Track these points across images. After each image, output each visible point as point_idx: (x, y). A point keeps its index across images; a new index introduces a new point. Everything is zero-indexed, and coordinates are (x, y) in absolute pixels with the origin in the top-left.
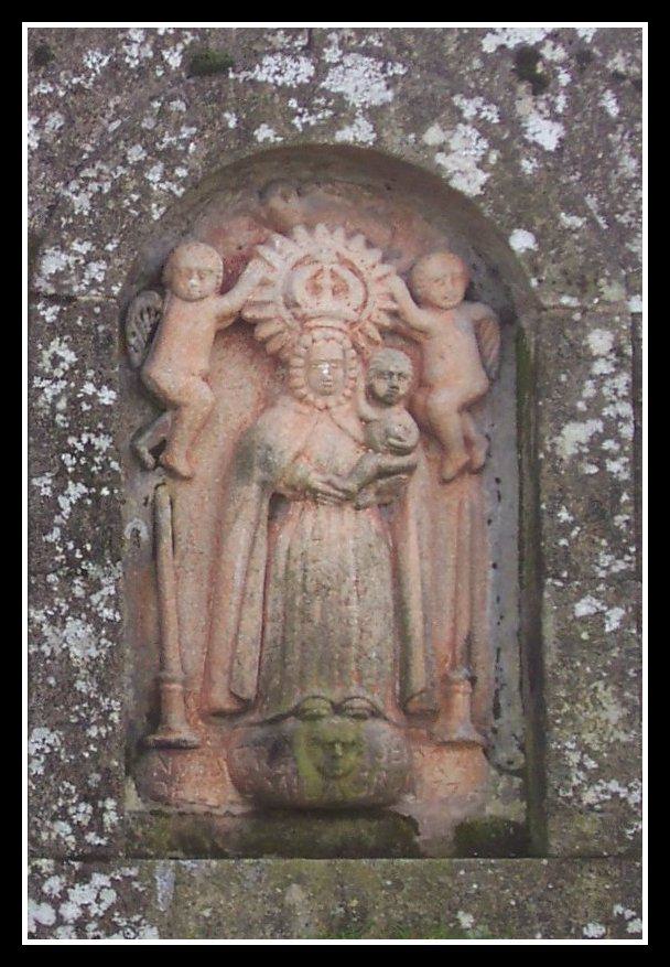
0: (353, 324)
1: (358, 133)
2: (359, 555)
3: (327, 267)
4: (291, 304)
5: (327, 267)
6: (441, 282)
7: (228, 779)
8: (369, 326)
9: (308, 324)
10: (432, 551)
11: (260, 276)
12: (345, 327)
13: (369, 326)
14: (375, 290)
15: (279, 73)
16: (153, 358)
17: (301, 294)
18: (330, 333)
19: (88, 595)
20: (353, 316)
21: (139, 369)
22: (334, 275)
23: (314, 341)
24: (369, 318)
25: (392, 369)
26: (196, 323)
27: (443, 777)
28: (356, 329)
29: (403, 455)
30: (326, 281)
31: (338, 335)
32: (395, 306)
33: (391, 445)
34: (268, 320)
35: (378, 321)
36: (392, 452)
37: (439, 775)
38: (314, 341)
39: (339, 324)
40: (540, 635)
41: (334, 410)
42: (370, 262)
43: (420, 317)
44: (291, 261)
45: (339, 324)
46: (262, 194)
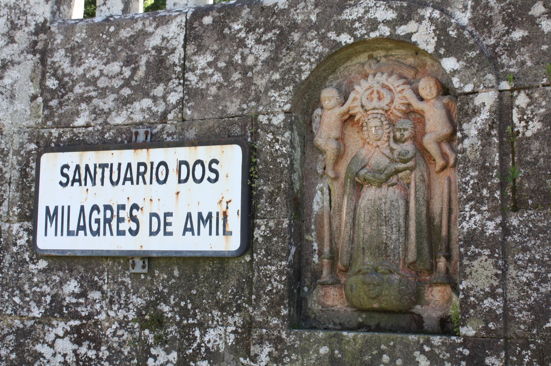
0: (386, 111)
1: (386, 31)
2: (387, 205)
3: (375, 89)
4: (362, 106)
5: (375, 89)
8: (394, 111)
10: (417, 200)
12: (383, 112)
13: (394, 111)
14: (397, 96)
15: (351, 15)
17: (365, 102)
18: (375, 115)
20: (387, 108)
22: (378, 92)
23: (368, 119)
25: (401, 127)
27: (433, 298)
28: (389, 113)
29: (405, 163)
30: (375, 95)
34: (357, 113)
36: (401, 162)
37: (431, 297)
38: (368, 119)
39: (380, 111)
40: (416, 239)
41: (380, 146)
42: (396, 84)
43: (417, 105)
45: (380, 111)
46: (168, 69)
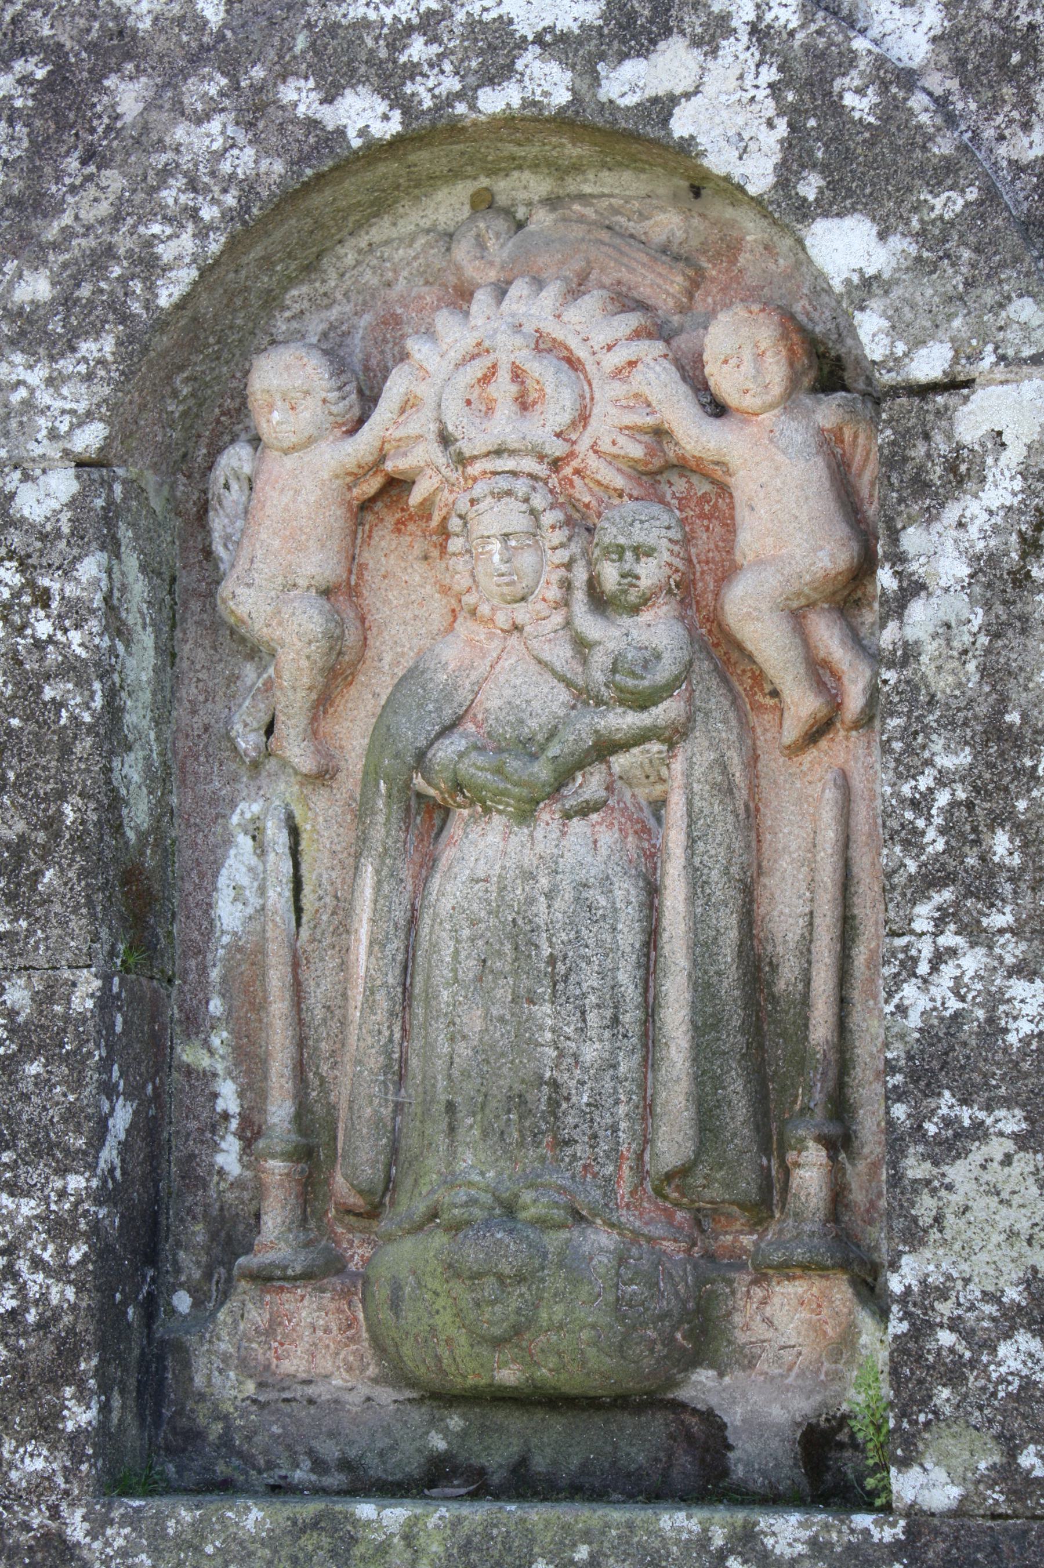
0: (556, 464)
2: (557, 904)
6: (733, 362)
7: (365, 1335)
8: (593, 463)
9: (470, 470)
11: (402, 390)
12: (541, 469)
13: (593, 463)
16: (839, 496)
17: (455, 418)
19: (900, 1070)
20: (557, 448)
21: (898, 532)
24: (594, 448)
26: (297, 492)
28: (568, 471)
29: (643, 708)
30: (503, 388)
31: (521, 486)
32: (650, 420)
33: (620, 689)
35: (614, 450)
36: (622, 702)
39: (529, 464)
44: (454, 355)
45: (529, 464)
